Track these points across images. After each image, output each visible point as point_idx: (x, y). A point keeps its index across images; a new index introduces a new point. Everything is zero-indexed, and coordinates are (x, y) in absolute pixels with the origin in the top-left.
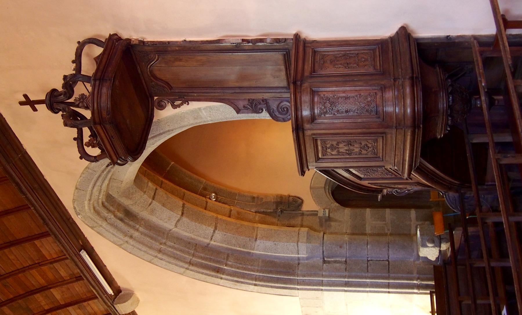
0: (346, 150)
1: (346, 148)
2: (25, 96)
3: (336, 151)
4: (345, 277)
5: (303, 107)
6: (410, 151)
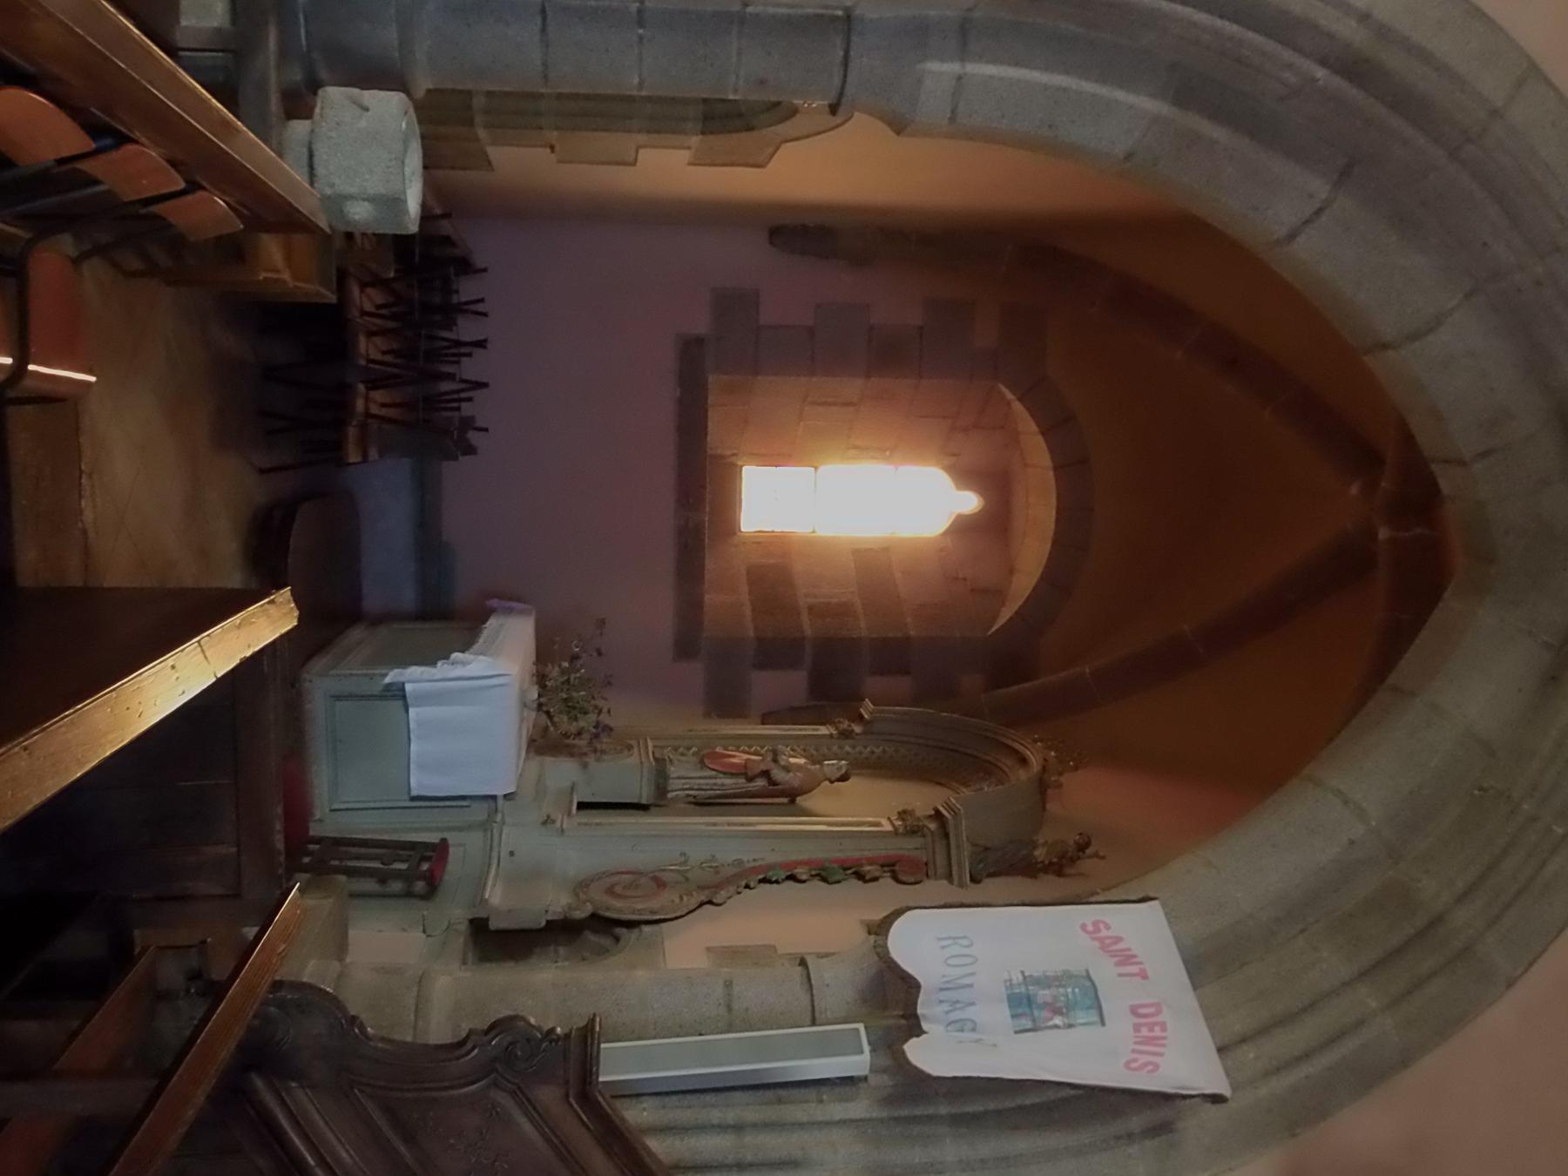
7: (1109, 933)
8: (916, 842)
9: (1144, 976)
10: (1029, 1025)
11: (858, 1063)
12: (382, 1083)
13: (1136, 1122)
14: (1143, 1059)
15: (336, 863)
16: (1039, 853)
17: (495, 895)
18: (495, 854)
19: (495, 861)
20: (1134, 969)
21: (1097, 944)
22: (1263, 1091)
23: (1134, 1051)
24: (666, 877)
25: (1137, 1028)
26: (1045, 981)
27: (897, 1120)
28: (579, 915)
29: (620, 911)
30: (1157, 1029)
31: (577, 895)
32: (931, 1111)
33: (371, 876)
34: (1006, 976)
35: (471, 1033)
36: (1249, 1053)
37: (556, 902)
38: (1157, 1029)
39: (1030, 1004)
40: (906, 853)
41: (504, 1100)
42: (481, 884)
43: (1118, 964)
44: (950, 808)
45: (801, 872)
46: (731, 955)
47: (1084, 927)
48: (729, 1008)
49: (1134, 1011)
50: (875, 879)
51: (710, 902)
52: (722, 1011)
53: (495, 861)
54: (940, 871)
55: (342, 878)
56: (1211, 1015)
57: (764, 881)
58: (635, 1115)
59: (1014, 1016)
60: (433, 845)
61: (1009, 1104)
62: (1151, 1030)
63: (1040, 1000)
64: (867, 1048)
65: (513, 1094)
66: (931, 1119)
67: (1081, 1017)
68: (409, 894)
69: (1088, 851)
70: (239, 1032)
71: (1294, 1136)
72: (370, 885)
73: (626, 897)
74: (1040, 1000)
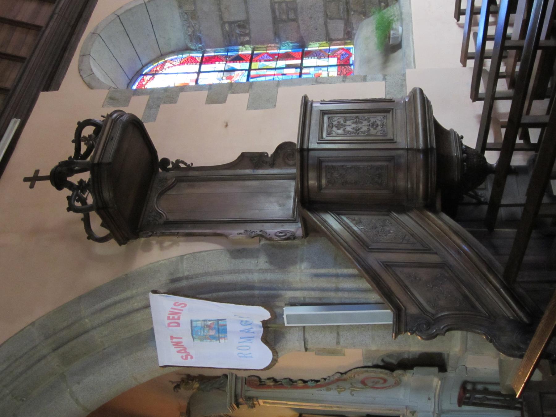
0: (353, 128)
1: (354, 126)
2: (26, 180)
3: (342, 129)
4: (340, 45)
5: (352, 238)
6: (421, 106)
7: (181, 355)
8: (249, 394)
9: (172, 338)
10: (220, 322)
11: (288, 311)
12: (478, 317)
13: (184, 283)
14: (179, 307)
15: (508, 399)
16: (196, 385)
17: (436, 382)
18: (437, 400)
19: (437, 396)
20: (175, 340)
21: (188, 351)
22: (134, 292)
23: (182, 310)
24: (361, 386)
25: (179, 318)
26: (212, 338)
27: (275, 289)
28: (399, 372)
29: (381, 373)
30: (171, 317)
31: (400, 380)
32: (262, 292)
33: (491, 392)
34: (226, 341)
35: (444, 335)
36: (137, 305)
37: (410, 377)
38: (171, 317)
39: (219, 330)
40: (253, 389)
41: (428, 308)
42: (442, 387)
43: (181, 342)
44: (233, 408)
45: (301, 384)
46: (332, 352)
47: (192, 358)
48: (338, 334)
49: (179, 325)
50: (269, 379)
51: (342, 374)
52: (341, 333)
53: (437, 396)
54: (240, 380)
55: (503, 392)
56: (149, 320)
57: (317, 381)
58: (375, 297)
59: (226, 325)
60: (465, 405)
61: (231, 293)
62: (173, 317)
63: (214, 331)
64: (285, 316)
65: (427, 311)
66: (261, 289)
67: (199, 324)
68: (474, 384)
69: (175, 384)
70: (535, 340)
71: (126, 275)
72: (491, 388)
73: (378, 378)
74: (214, 331)
